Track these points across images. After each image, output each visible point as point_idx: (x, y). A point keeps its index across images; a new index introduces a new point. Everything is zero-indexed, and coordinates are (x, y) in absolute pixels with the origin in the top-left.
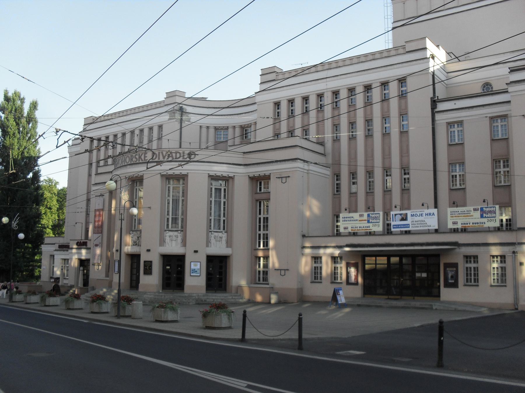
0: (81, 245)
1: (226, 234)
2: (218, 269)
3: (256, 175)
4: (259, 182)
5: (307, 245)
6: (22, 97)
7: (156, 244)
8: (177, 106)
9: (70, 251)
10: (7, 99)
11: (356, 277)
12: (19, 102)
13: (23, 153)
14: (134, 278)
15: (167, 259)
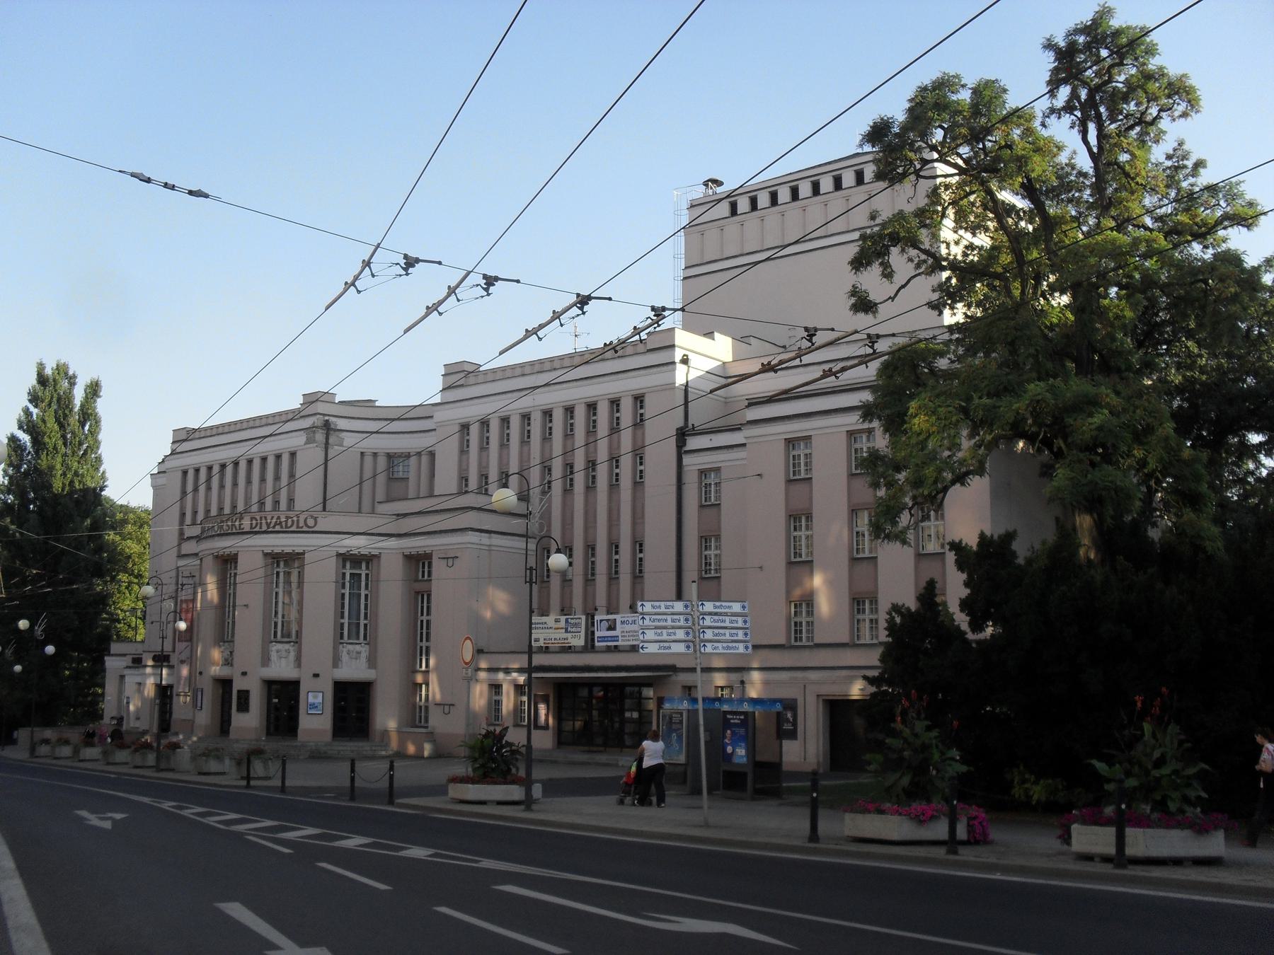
0: (161, 659)
2: (353, 703)
3: (414, 552)
4: (419, 563)
5: (483, 665)
6: (71, 373)
8: (320, 419)
9: (141, 671)
10: (42, 380)
11: (547, 720)
12: (66, 384)
13: (72, 482)
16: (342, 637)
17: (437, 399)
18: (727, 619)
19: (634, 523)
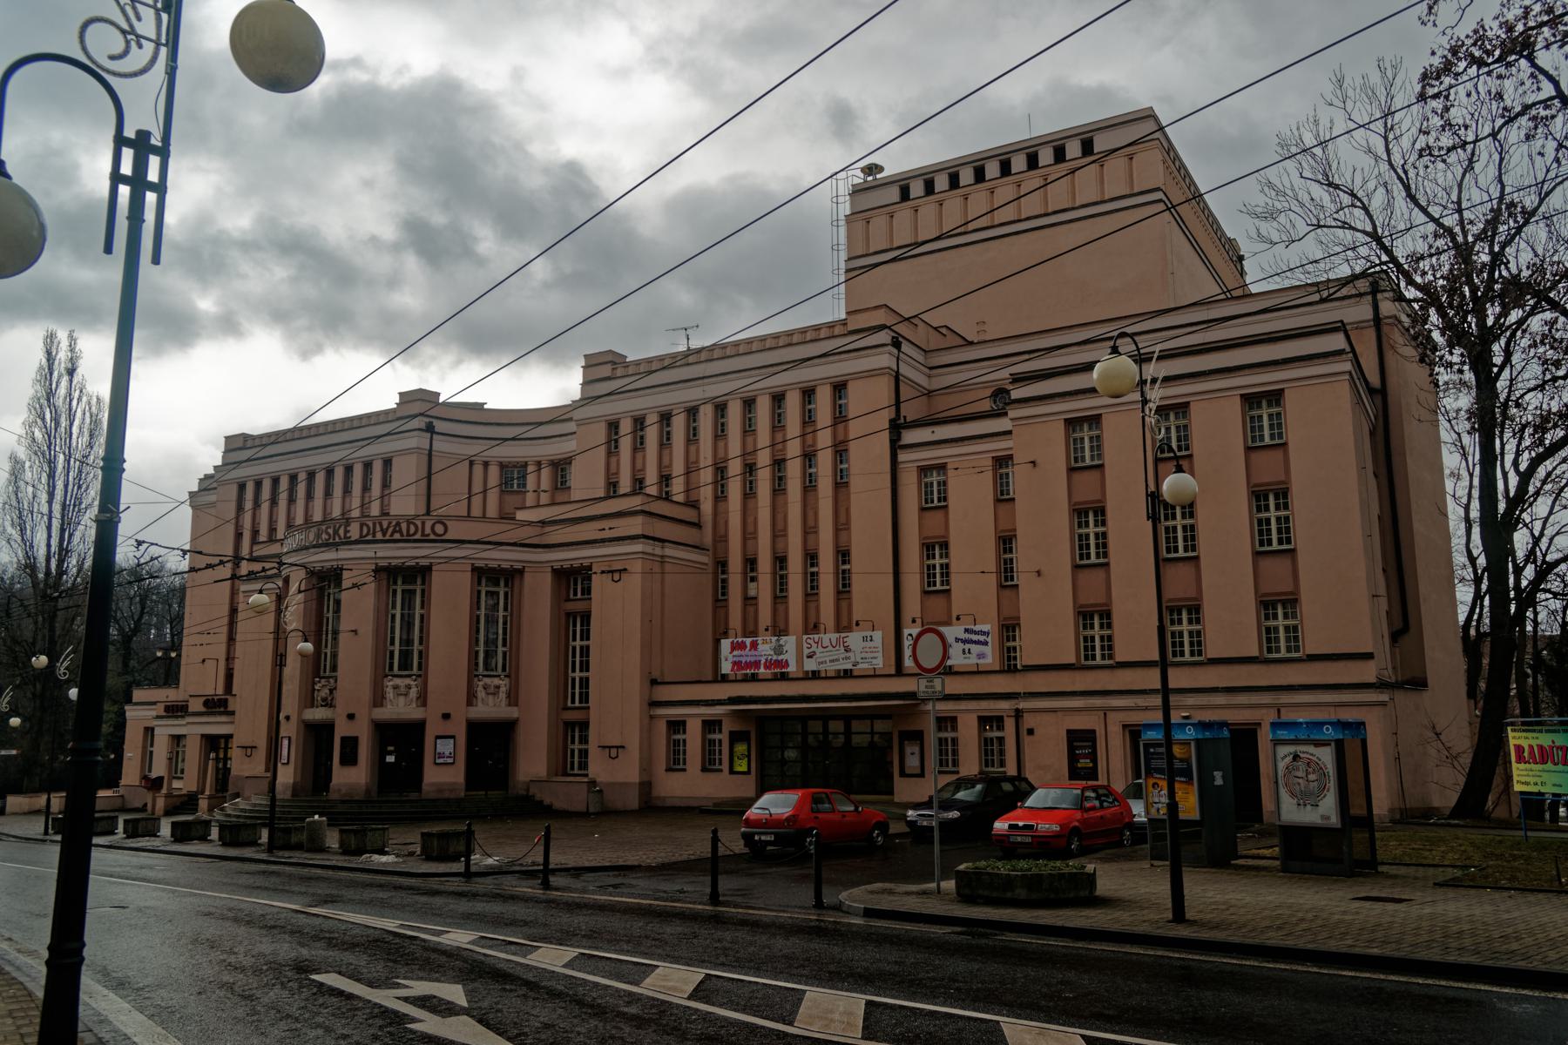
2: (490, 744)
3: (566, 565)
4: (573, 580)
7: (354, 706)
17: (833, 309)
19: (745, 539)
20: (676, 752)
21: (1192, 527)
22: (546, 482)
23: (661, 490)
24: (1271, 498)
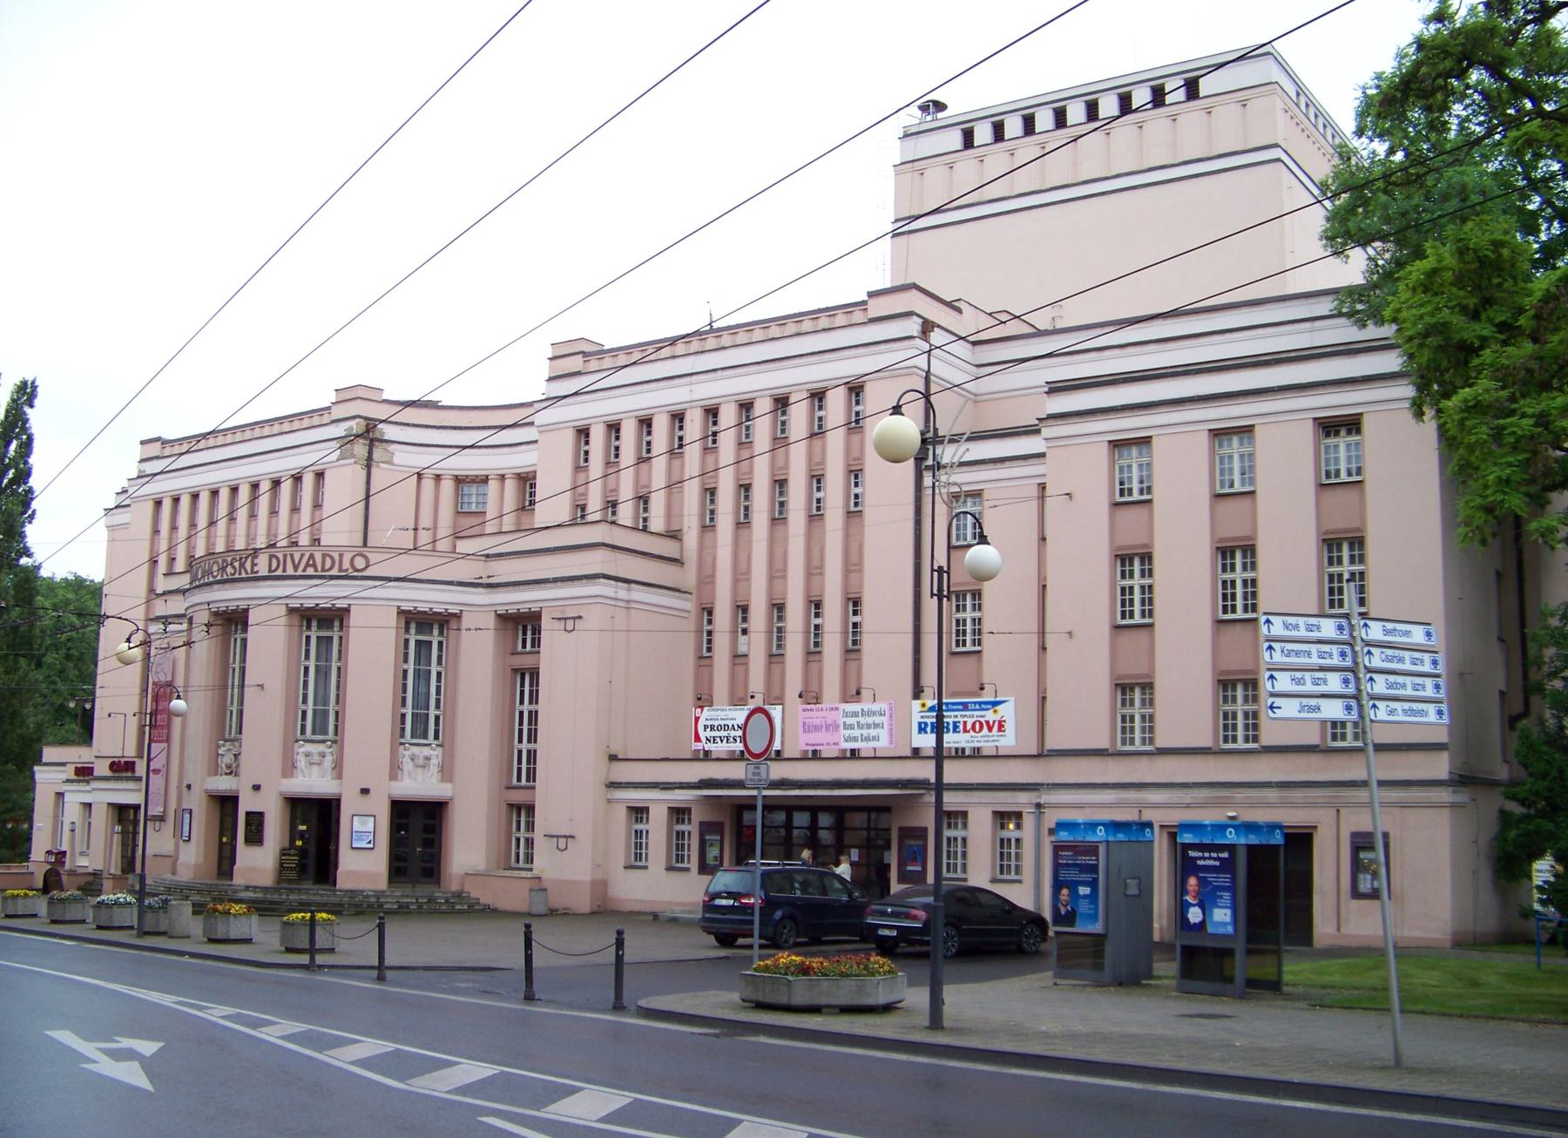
1: (440, 750)
2: (418, 828)
3: (512, 610)
4: (522, 626)
7: (271, 776)
14: (227, 853)
15: (298, 806)
16: (402, 736)
18: (1407, 655)
19: (736, 581)
20: (638, 846)
21: (1254, 581)
22: (510, 502)
23: (636, 517)
24: (1345, 547)
